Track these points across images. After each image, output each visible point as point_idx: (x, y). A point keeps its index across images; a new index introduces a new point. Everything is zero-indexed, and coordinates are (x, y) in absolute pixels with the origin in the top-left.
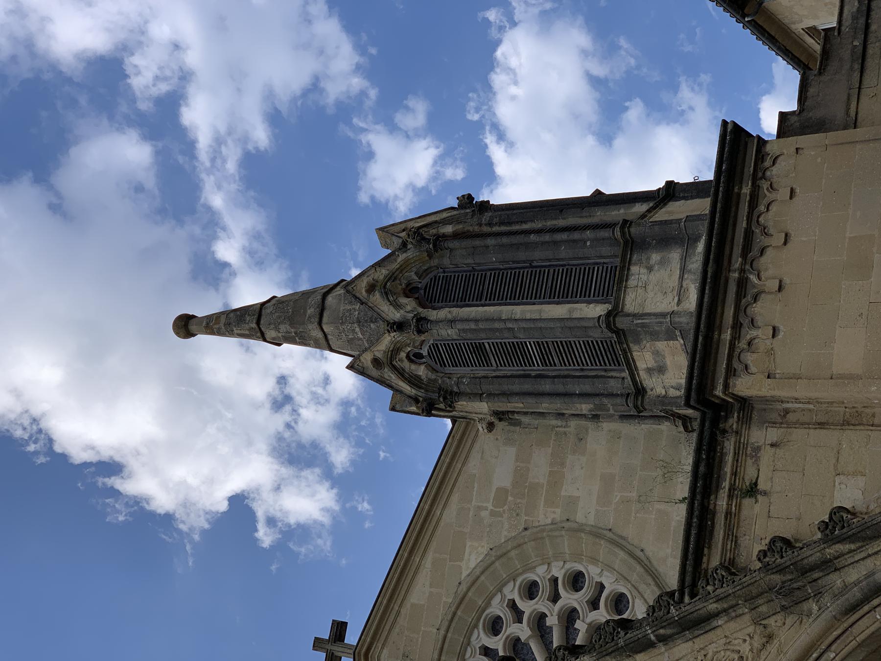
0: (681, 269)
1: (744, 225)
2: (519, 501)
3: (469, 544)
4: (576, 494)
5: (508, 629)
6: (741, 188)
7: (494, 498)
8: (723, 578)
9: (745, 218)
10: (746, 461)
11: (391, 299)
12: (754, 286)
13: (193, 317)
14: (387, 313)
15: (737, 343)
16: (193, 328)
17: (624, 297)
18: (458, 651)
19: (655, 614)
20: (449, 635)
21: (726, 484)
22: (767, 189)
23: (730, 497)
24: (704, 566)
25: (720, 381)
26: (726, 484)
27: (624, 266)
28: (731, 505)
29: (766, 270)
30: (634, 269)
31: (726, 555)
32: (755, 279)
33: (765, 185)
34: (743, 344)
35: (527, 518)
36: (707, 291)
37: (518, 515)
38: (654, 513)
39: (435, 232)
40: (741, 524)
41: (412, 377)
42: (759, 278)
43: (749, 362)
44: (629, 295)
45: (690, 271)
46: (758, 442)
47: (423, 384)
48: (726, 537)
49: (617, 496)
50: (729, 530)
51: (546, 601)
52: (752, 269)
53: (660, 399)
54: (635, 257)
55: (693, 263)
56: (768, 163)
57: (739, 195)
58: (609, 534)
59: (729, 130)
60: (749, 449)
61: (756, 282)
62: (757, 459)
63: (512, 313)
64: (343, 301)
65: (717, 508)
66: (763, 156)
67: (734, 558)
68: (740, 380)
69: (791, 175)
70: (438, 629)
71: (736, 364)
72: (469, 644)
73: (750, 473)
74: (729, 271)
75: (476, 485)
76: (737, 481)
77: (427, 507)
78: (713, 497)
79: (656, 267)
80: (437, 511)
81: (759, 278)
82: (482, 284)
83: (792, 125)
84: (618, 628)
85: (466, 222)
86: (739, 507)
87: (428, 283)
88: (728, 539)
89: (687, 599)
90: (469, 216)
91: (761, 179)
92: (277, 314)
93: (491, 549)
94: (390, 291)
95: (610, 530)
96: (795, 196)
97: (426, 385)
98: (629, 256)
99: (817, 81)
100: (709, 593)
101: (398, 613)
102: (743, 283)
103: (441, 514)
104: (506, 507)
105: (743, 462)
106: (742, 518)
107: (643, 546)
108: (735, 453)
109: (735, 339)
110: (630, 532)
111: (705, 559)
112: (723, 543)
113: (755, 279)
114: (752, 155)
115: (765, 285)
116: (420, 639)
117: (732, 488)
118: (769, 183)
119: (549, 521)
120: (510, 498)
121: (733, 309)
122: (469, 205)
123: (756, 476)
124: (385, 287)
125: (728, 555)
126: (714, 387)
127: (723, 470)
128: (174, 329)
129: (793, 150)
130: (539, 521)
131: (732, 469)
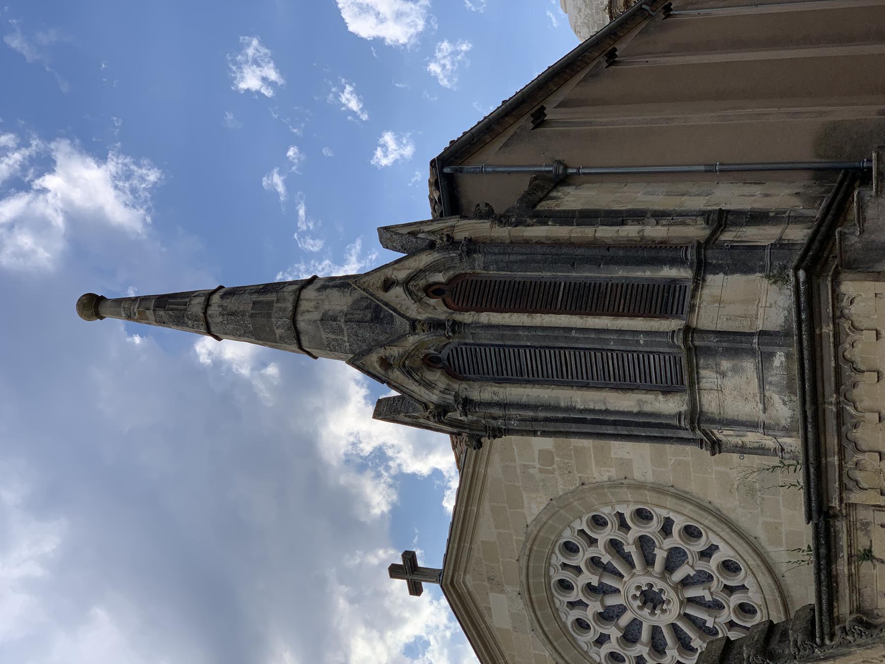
0: (759, 378)
1: (833, 364)
2: (567, 461)
3: (525, 495)
4: (627, 456)
5: (586, 553)
6: (821, 329)
7: (539, 458)
8: (861, 633)
9: (833, 359)
10: (857, 533)
11: (417, 377)
12: (852, 417)
13: (102, 298)
14: (419, 393)
15: (843, 463)
16: (102, 309)
17: (700, 398)
18: (543, 573)
19: (801, 653)
20: (531, 564)
21: (845, 554)
22: (849, 329)
23: (849, 563)
24: (836, 615)
25: (836, 495)
26: (845, 554)
27: (692, 370)
28: (851, 569)
29: (861, 401)
30: (703, 372)
31: (853, 604)
32: (852, 411)
33: (846, 325)
34: (850, 465)
35: (581, 475)
36: (810, 430)
37: (570, 472)
38: (714, 474)
39: (424, 283)
40: (861, 579)
41: (451, 421)
42: (856, 408)
43: (859, 479)
44: (704, 396)
45: (770, 383)
46: (865, 519)
47: (465, 424)
48: (851, 592)
49: (671, 459)
50: (853, 586)
51: (617, 531)
52: (847, 400)
53: (738, 449)
54: (702, 361)
55: (772, 376)
56: (845, 303)
57: (821, 335)
58: (672, 490)
59: (801, 280)
60: (858, 524)
61: (854, 413)
62: (867, 533)
63: (572, 402)
64: (322, 329)
65: (839, 571)
66: (838, 295)
67: (860, 604)
68: (853, 494)
69: (872, 317)
70: (517, 560)
71: (846, 480)
72: (550, 564)
73: (862, 542)
74: (824, 403)
75: (515, 447)
76: (853, 550)
77: (471, 470)
78: (834, 566)
79: (730, 374)
80: (481, 470)
81: (856, 408)
82: (517, 358)
83: (852, 245)
84: (766, 659)
85: (455, 267)
86: (858, 568)
87: (449, 354)
88: (853, 592)
89: (827, 642)
90: (457, 260)
91: (840, 317)
92: (232, 326)
93: (551, 500)
94: (411, 367)
95: (672, 486)
96: (881, 337)
97: (468, 425)
98: (695, 361)
99: (875, 203)
100: (850, 642)
101: (470, 549)
102: (840, 415)
103: (486, 471)
104: (555, 466)
105: (855, 535)
106: (861, 575)
107: (709, 499)
108: (848, 531)
109: (842, 460)
110: (693, 488)
111: (835, 610)
112: (850, 598)
113: (852, 411)
114: (828, 293)
115: (863, 417)
116: (501, 567)
117: (850, 556)
118: (850, 322)
119: (605, 478)
120: (556, 459)
121: (836, 438)
122: (451, 247)
123: (869, 544)
124: (404, 366)
125: (855, 604)
126: (829, 501)
127: (838, 543)
128: (81, 316)
129: (872, 295)
130: (595, 478)
131: (847, 542)
